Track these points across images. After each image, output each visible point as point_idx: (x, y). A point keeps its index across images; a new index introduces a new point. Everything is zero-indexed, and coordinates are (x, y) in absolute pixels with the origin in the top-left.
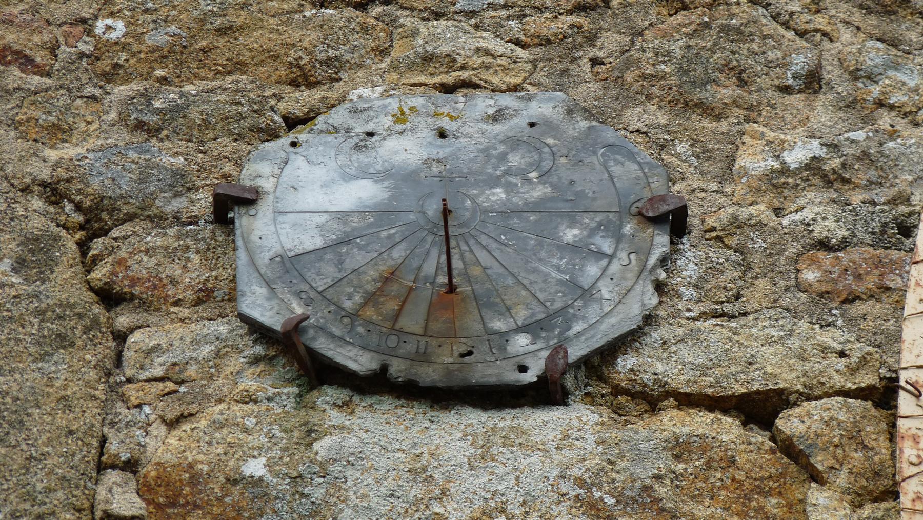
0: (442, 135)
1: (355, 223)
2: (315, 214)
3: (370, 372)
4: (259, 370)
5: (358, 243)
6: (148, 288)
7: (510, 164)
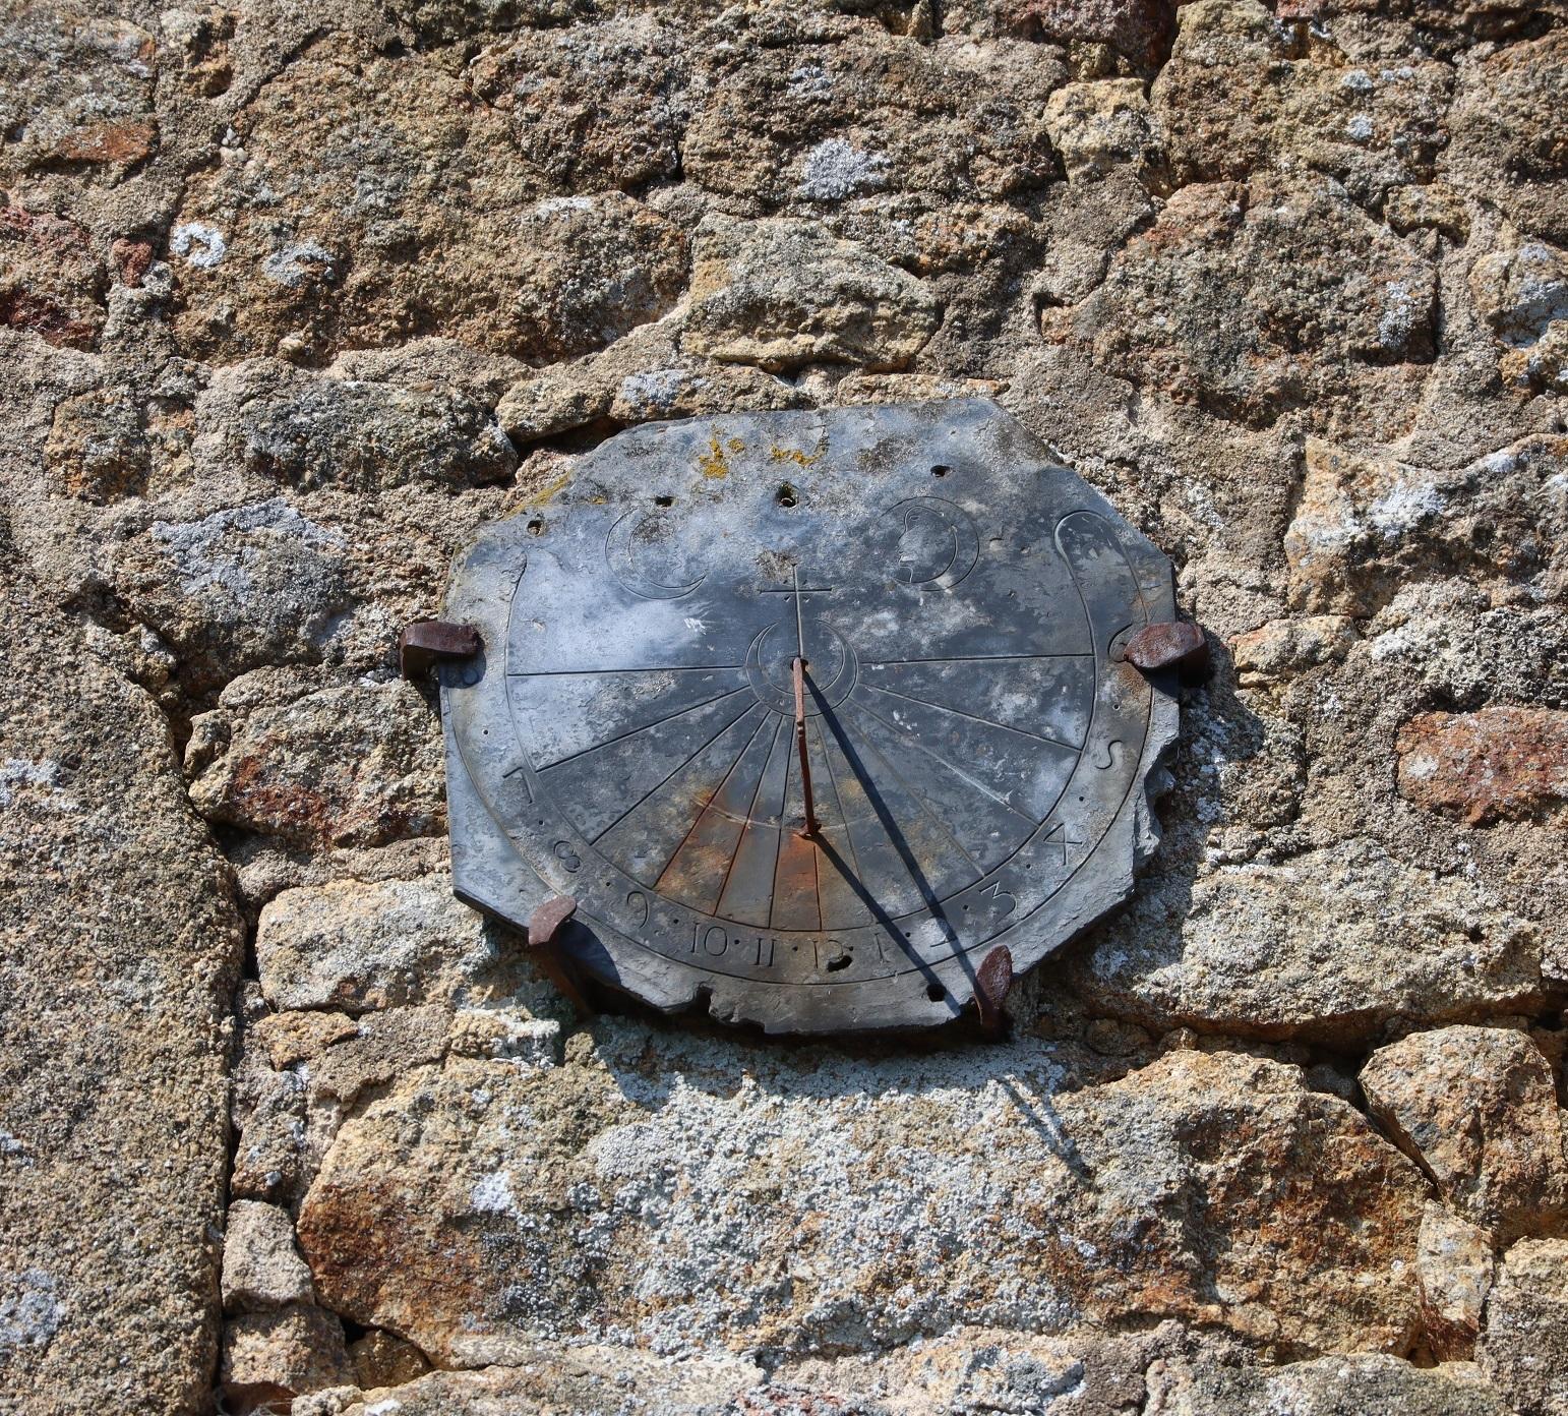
1: (647, 688)
6: (294, 813)
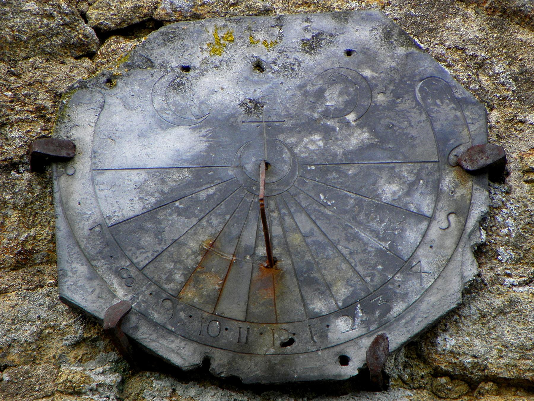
0: (258, 66)
2: (133, 172)
3: (192, 367)
4: (81, 354)
5: (177, 207)
7: (328, 104)
